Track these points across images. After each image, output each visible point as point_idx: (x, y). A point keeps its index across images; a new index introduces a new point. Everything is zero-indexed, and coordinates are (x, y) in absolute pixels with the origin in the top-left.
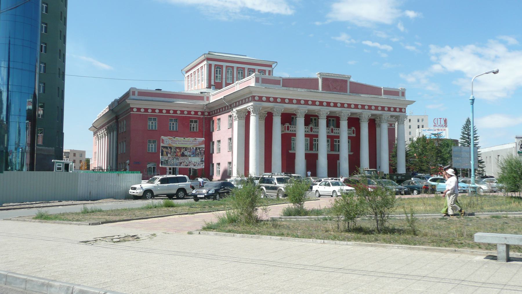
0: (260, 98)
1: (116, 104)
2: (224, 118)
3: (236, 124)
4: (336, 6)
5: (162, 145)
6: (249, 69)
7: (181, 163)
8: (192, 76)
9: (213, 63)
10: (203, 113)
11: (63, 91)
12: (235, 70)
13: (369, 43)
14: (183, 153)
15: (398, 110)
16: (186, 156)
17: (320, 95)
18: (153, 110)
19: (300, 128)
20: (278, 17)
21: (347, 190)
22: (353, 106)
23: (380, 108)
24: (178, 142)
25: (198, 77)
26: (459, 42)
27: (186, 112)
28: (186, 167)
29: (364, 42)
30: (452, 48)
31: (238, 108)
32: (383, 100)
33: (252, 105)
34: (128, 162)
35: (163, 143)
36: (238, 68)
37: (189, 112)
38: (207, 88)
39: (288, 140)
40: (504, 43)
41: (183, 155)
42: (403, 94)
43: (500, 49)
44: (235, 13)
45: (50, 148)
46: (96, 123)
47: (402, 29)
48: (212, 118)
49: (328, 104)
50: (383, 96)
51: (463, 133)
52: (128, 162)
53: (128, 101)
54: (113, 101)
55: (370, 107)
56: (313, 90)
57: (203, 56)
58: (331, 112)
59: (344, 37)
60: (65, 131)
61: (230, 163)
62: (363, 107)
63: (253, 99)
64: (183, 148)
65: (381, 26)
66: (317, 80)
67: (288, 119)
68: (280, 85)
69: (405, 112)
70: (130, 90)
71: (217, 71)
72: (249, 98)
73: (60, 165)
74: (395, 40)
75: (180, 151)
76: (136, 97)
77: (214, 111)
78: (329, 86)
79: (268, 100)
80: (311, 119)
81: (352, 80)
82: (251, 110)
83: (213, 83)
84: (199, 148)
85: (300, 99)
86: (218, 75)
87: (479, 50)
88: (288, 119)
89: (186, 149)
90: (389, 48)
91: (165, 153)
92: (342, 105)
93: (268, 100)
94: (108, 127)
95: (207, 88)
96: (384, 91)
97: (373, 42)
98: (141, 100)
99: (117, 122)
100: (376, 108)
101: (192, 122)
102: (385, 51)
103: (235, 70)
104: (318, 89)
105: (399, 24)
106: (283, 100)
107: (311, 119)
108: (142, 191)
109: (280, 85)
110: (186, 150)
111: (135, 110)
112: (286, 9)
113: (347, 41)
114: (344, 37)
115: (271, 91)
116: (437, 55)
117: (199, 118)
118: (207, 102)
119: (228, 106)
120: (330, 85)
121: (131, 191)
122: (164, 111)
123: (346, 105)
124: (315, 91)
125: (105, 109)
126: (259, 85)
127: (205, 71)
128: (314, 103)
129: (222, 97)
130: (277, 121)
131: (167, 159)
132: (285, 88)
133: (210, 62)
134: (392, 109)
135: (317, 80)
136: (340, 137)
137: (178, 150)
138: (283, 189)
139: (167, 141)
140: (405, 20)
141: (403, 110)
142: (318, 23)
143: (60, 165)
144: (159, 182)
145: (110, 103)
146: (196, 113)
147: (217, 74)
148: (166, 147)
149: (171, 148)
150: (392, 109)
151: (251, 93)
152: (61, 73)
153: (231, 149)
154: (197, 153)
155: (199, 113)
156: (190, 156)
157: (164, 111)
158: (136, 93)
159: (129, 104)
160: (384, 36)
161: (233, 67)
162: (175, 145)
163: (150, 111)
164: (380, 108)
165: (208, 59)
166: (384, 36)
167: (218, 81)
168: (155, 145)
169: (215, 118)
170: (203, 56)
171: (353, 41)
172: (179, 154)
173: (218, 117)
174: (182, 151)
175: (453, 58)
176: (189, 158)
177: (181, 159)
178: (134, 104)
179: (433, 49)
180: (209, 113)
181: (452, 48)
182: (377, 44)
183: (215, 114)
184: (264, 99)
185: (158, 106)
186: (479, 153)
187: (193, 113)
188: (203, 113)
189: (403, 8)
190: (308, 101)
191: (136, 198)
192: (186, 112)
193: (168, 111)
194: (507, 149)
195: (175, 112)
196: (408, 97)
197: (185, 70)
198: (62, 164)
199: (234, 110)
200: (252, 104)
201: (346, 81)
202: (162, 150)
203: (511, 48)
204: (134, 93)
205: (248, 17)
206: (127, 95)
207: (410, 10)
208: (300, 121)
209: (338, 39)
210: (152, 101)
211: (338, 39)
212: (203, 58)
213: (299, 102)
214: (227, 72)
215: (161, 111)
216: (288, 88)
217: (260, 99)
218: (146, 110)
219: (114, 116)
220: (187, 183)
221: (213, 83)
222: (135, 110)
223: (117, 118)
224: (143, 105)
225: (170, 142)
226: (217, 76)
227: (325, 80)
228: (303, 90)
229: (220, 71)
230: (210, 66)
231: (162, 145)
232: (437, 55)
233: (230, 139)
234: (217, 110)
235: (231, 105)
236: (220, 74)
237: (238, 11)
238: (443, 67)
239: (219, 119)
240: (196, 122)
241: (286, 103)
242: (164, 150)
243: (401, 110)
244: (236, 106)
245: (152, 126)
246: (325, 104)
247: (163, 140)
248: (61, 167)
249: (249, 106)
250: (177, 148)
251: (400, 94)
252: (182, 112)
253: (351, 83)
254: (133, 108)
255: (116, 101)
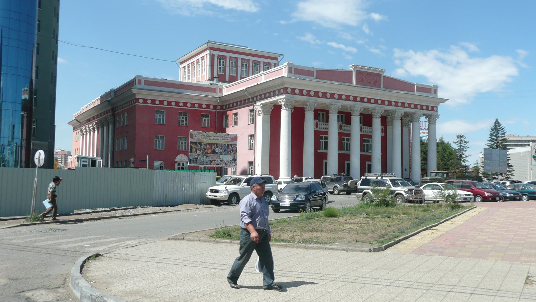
0: (293, 90)
1: (113, 95)
2: (243, 113)
3: (260, 119)
4: (301, 5)
5: (190, 140)
6: (254, 61)
7: (211, 162)
8: (189, 67)
9: (217, 53)
10: (215, 107)
11: (55, 77)
12: (239, 61)
13: (334, 44)
14: (214, 150)
15: (430, 108)
16: (217, 153)
17: (354, 89)
18: (161, 102)
19: (333, 127)
20: (242, 14)
21: (466, 195)
22: (386, 103)
23: (413, 106)
24: (208, 138)
25: (198, 68)
26: (422, 45)
27: (197, 106)
28: (217, 166)
29: (329, 44)
30: (416, 53)
31: (263, 102)
32: (415, 98)
33: (284, 98)
34: (132, 159)
35: (192, 137)
36: (242, 59)
37: (200, 106)
38: (209, 80)
39: (320, 139)
40: (464, 48)
41: (214, 152)
42: (435, 92)
43: (462, 56)
44: (198, 8)
45: (43, 142)
46: (81, 116)
47: (367, 31)
48: (226, 112)
49: (362, 100)
50: (416, 93)
51: (491, 135)
52: (132, 159)
53: (134, 91)
54: (108, 90)
55: (403, 104)
56: (347, 84)
57: (206, 45)
58: (365, 109)
59: (309, 37)
60: (56, 123)
61: (251, 163)
62: (396, 104)
63: (285, 91)
64: (214, 144)
65: (347, 28)
66: (351, 72)
67: (321, 115)
68: (313, 76)
69: (437, 111)
70: (135, 79)
71: (220, 61)
72: (279, 90)
73: (86, 162)
74: (360, 42)
75: (211, 148)
76: (142, 86)
77: (229, 105)
78: (363, 80)
79: (301, 92)
80: (345, 117)
81: (386, 74)
82: (283, 103)
83: (215, 75)
84: (231, 145)
85: (334, 92)
86: (221, 67)
87: (442, 55)
88: (321, 115)
89: (217, 145)
90: (354, 50)
91: (194, 150)
92: (376, 101)
93: (301, 92)
94: (101, 121)
95: (209, 80)
96: (417, 87)
97: (338, 43)
98: (148, 90)
99: (114, 115)
100: (409, 105)
101: (203, 116)
102: (348, 53)
103: (239, 61)
104: (352, 83)
105: (364, 26)
106: (316, 94)
107: (345, 117)
108: (227, 194)
109: (313, 76)
110: (217, 147)
111: (141, 101)
112: (251, 6)
113: (312, 42)
114: (309, 37)
115: (305, 82)
116: (401, 59)
117: (211, 112)
118: (219, 95)
119: (249, 99)
120: (364, 79)
121: (209, 193)
122: (173, 104)
123: (379, 102)
124: (349, 84)
125: (95, 101)
126: (292, 75)
127: (207, 61)
128: (348, 98)
129: (244, 88)
130: (309, 117)
131: (196, 157)
132: (319, 80)
133: (213, 52)
134: (425, 108)
135: (351, 72)
136: (373, 137)
137: (208, 147)
138: (403, 193)
139: (196, 135)
140: (371, 23)
141: (435, 109)
142: (283, 22)
143: (86, 162)
144: (246, 184)
145: (103, 93)
146: (208, 106)
147: (220, 65)
148: (195, 143)
149: (200, 144)
150: (425, 108)
151: (283, 84)
152: (55, 56)
153: (252, 146)
154: (229, 150)
155: (211, 107)
156: (221, 154)
157: (173, 104)
158: (143, 82)
159: (135, 94)
160: (349, 38)
161: (237, 59)
162: (205, 141)
163: (157, 102)
164: (413, 106)
165: (211, 49)
166: (349, 38)
167: (221, 73)
168: (163, 142)
169: (230, 113)
170: (206, 45)
171: (318, 42)
172: (210, 151)
173: (235, 111)
174: (213, 148)
175: (416, 63)
176: (221, 156)
177: (212, 157)
178: (139, 93)
179: (397, 53)
180: (222, 107)
181: (416, 53)
182: (342, 46)
183: (229, 107)
184: (297, 91)
185: (166, 97)
186: (508, 156)
187: (204, 106)
188: (215, 107)
189: (369, 11)
190: (342, 95)
191: (216, 202)
192: (197, 106)
193: (177, 104)
194: (520, 153)
195: (185, 104)
196: (440, 94)
197: (180, 60)
198: (88, 160)
199: (258, 103)
200: (284, 96)
201: (380, 75)
202: (191, 146)
203: (472, 55)
204: (140, 82)
205: (211, 13)
206: (131, 84)
207: (376, 12)
208: (334, 118)
209: (303, 38)
210: (160, 91)
211: (303, 38)
212: (205, 46)
213: (332, 96)
214: (231, 63)
215: (169, 103)
216: (321, 81)
217: (293, 91)
218: (153, 101)
219: (110, 107)
220: (273, 184)
221: (215, 75)
222: (141, 101)
223: (113, 110)
224: (150, 96)
225: (200, 137)
226: (220, 68)
227: (359, 73)
228: (338, 83)
229: (226, 62)
230: (213, 56)
231: (190, 140)
232: (401, 59)
233: (252, 136)
234: (233, 104)
235: (253, 98)
236: (223, 65)
237: (200, 6)
238: (407, 71)
239: (236, 114)
240: (207, 116)
241: (319, 97)
242: (194, 146)
243: (433, 107)
244: (261, 99)
245: (160, 119)
246: (359, 99)
247: (192, 134)
248: (87, 163)
249: (281, 99)
250: (207, 144)
251: (433, 91)
252: (193, 105)
253: (384, 77)
254: (139, 99)
255: (112, 91)
